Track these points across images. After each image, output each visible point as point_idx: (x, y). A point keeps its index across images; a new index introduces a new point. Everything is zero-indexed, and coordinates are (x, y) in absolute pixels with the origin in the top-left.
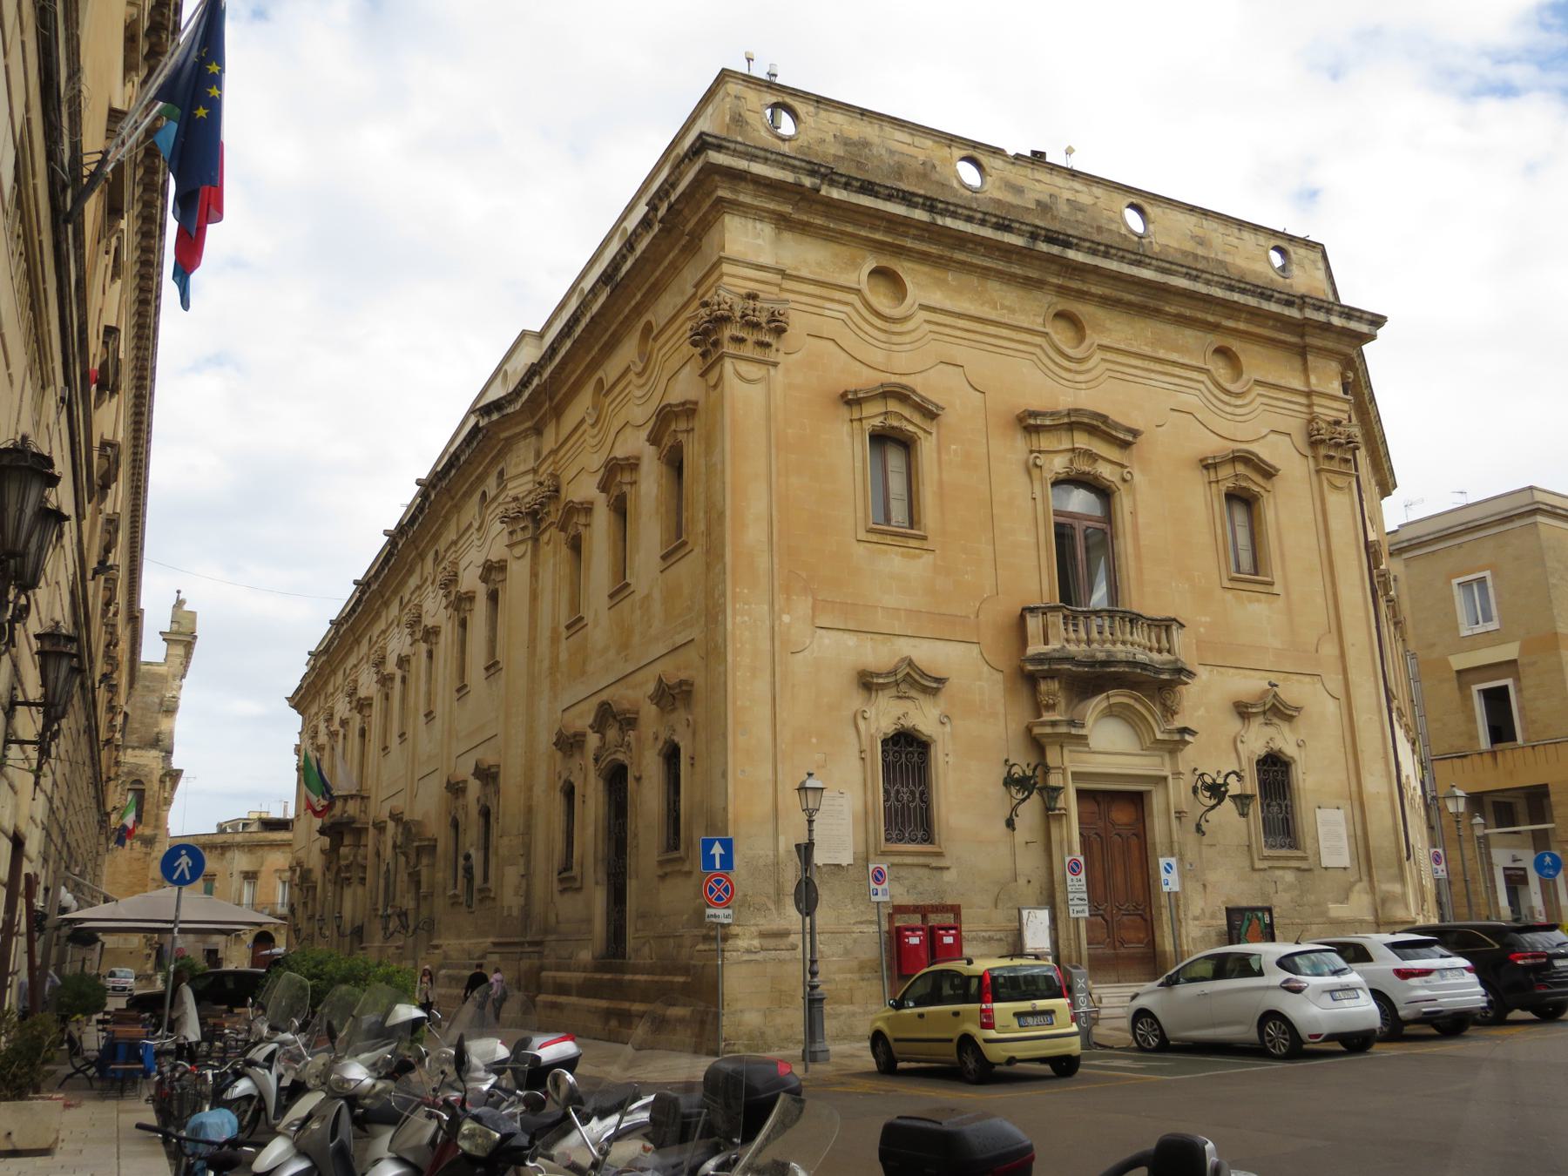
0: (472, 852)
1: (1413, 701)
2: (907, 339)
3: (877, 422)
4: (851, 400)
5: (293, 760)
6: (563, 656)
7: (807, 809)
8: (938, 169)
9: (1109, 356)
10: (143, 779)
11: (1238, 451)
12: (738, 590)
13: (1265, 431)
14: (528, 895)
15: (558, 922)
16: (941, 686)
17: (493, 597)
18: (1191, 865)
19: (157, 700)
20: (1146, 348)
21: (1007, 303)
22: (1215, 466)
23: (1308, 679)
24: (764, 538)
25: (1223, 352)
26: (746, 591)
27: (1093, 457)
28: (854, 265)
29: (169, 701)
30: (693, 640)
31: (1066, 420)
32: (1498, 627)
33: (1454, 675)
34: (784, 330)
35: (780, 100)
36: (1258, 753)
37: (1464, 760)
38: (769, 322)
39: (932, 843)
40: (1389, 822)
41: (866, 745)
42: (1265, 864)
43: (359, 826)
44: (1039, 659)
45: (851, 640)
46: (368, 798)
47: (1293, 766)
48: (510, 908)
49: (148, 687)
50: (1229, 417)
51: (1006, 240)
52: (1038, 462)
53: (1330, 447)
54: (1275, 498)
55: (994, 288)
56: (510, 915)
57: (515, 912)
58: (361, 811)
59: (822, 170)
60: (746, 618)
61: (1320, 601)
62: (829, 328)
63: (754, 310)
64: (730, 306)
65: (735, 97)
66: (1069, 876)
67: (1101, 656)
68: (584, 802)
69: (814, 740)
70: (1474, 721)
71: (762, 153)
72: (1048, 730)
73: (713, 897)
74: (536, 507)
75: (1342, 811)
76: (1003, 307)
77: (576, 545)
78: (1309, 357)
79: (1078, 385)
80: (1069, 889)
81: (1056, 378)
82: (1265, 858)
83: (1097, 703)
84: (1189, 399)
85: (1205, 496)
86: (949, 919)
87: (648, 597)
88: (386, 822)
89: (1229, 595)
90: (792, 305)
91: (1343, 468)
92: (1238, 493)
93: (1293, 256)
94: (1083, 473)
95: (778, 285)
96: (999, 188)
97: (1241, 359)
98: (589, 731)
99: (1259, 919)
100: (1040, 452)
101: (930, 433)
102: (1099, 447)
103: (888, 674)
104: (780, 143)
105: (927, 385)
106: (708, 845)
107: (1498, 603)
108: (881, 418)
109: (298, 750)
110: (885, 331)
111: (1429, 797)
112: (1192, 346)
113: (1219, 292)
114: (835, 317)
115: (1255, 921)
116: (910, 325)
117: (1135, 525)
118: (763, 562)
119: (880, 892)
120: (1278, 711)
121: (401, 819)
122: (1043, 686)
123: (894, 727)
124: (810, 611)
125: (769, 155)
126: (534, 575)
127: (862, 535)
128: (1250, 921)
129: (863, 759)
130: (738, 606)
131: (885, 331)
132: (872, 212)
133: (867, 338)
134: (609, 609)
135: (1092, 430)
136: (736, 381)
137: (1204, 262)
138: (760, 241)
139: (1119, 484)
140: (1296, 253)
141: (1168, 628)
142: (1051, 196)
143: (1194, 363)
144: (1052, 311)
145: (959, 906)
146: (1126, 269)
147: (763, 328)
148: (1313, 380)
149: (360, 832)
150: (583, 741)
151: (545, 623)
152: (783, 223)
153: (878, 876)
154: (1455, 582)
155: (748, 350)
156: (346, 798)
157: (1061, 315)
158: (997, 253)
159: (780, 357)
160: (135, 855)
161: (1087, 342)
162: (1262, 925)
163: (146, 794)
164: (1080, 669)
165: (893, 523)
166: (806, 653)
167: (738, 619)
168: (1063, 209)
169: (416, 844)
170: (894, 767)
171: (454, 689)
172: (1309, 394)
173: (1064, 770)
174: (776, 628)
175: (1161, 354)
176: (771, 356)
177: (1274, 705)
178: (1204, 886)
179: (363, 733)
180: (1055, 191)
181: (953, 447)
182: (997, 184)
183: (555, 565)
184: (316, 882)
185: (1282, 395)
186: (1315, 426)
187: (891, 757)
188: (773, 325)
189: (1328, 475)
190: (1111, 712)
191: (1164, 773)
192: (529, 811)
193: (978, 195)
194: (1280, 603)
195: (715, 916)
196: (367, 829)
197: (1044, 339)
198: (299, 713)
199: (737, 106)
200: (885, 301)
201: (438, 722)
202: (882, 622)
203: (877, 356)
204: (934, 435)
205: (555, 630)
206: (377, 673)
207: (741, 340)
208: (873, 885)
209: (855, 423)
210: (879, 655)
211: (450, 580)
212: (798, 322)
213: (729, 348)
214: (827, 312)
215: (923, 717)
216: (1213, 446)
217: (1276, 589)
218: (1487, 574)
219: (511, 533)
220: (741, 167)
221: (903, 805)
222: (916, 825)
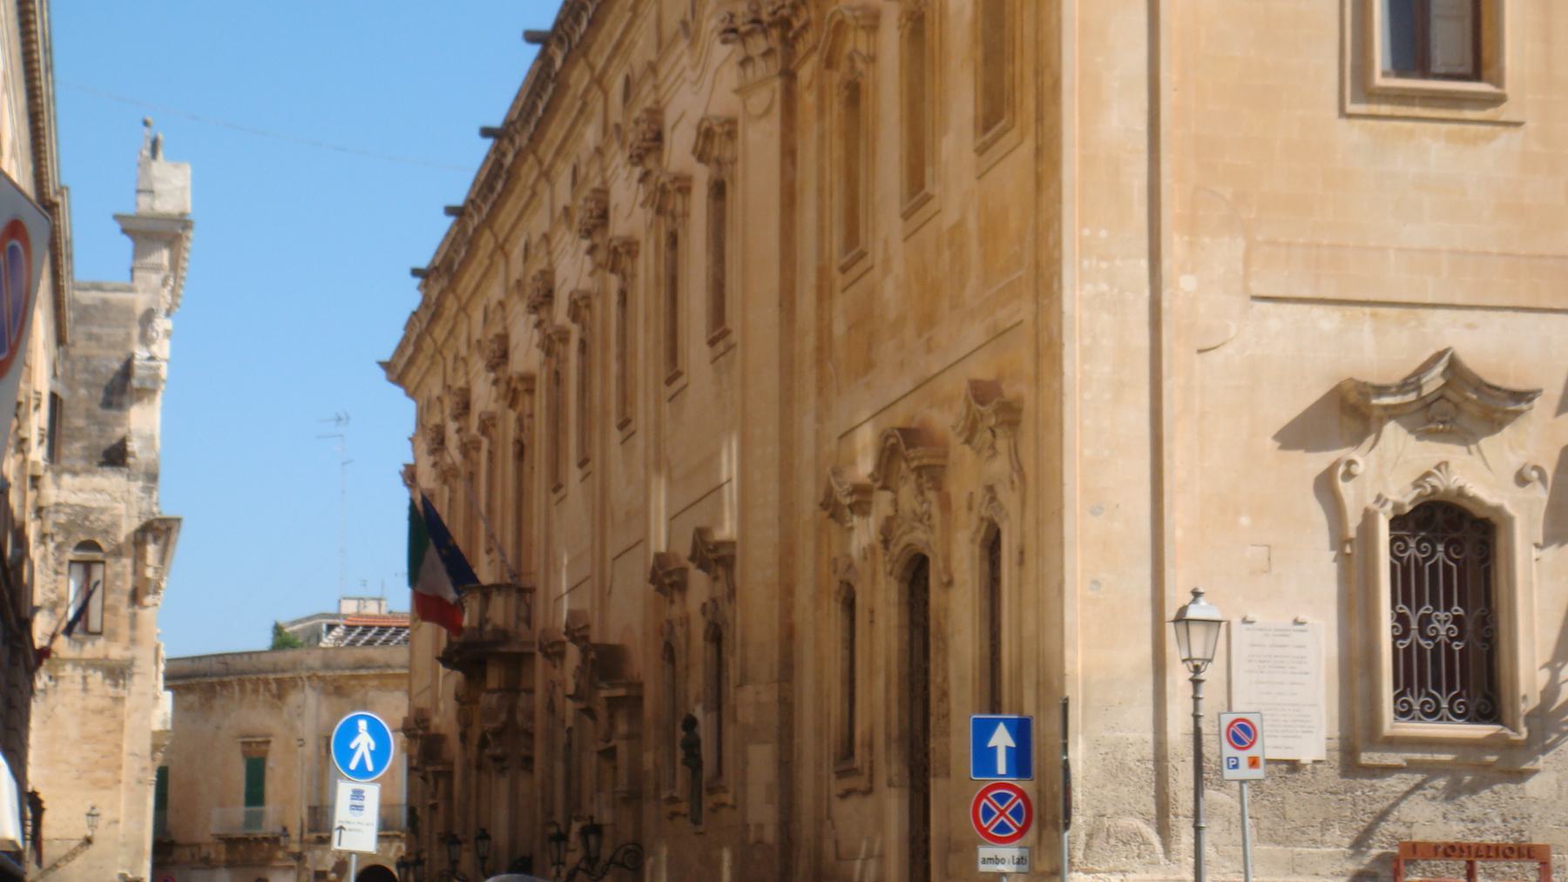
0: (699, 713)
5: (400, 500)
6: (839, 328)
7: (1190, 659)
10: (98, 540)
15: (838, 857)
17: (719, 190)
26: (1103, 233)
30: (1021, 322)
43: (516, 649)
45: (1327, 320)
46: (532, 590)
48: (760, 827)
56: (760, 842)
58: (518, 617)
68: (872, 622)
69: (1245, 521)
73: (990, 825)
77: (854, 93)
87: (959, 226)
88: (562, 643)
98: (692, 567)
106: (984, 730)
109: (410, 476)
121: (586, 638)
124: (1240, 266)
126: (789, 153)
134: (905, 240)
149: (518, 662)
150: (943, 467)
156: (486, 592)
160: (94, 701)
166: (1228, 350)
169: (604, 693)
170: (1419, 571)
171: (663, 378)
179: (521, 451)
183: (822, 137)
184: (451, 764)
187: (1412, 551)
192: (788, 635)
195: (996, 860)
196: (532, 655)
201: (639, 442)
205: (822, 272)
206: (539, 325)
219: (745, 62)
221: (1438, 645)
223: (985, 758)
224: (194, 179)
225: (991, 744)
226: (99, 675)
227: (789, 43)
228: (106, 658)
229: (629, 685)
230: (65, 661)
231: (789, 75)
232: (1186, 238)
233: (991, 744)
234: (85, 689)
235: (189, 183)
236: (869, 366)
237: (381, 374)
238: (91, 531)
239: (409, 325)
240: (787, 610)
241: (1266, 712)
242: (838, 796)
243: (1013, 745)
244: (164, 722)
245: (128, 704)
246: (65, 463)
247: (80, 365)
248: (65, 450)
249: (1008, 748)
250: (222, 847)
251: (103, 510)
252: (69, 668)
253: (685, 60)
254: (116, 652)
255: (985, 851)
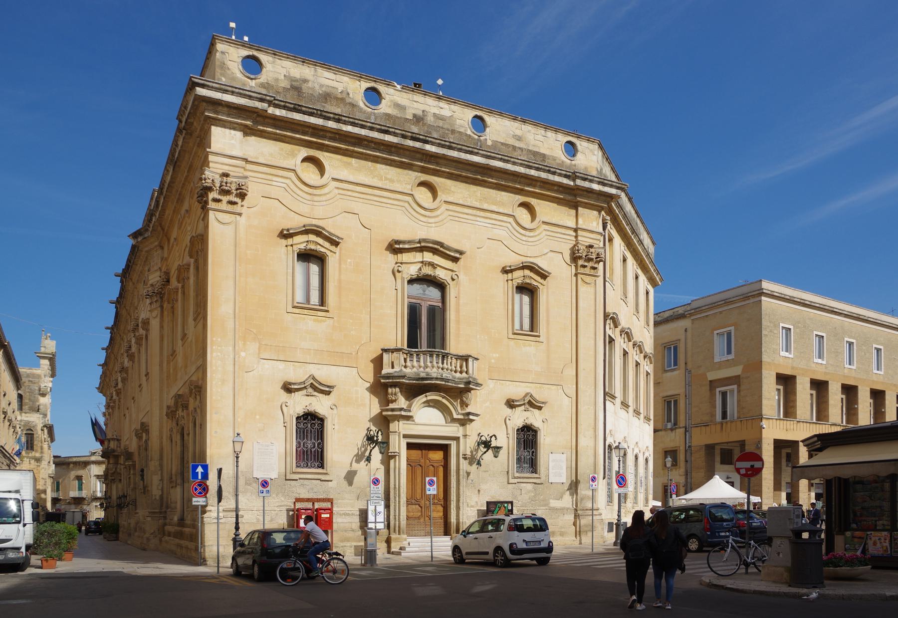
1: (686, 396)
2: (324, 198)
3: (302, 246)
4: (285, 235)
8: (351, 95)
9: (451, 207)
11: (526, 262)
12: (214, 339)
13: (546, 251)
14: (162, 490)
15: (171, 503)
16: (331, 390)
18: (472, 481)
19: (37, 388)
20: (475, 203)
21: (389, 177)
22: (511, 271)
23: (555, 387)
24: (231, 311)
25: (524, 205)
26: (219, 340)
27: (433, 265)
28: (293, 155)
29: (43, 388)
31: (418, 245)
32: (734, 357)
33: (708, 382)
34: (246, 195)
35: (251, 53)
36: (518, 425)
37: (707, 427)
38: (237, 190)
39: (323, 468)
40: (591, 460)
41: (287, 419)
42: (516, 481)
43: (116, 454)
44: (388, 377)
45: (281, 365)
47: (539, 433)
48: (155, 495)
49: (32, 381)
50: (524, 243)
51: (386, 139)
52: (400, 269)
53: (585, 261)
54: (547, 289)
55: (381, 168)
56: (155, 499)
57: (158, 498)
59: (268, 98)
60: (219, 354)
61: (568, 346)
62: (275, 192)
63: (226, 183)
64: (213, 180)
65: (222, 52)
66: (428, 486)
67: (423, 375)
69: (258, 417)
70: (715, 407)
71: (230, 89)
72: (390, 413)
74: (160, 290)
75: (565, 455)
76: (386, 179)
78: (579, 208)
79: (430, 225)
80: (372, 492)
81: (417, 221)
82: (515, 478)
83: (422, 399)
84: (501, 233)
85: (504, 288)
86: (327, 505)
89: (512, 343)
90: (251, 179)
91: (592, 272)
92: (526, 286)
93: (579, 147)
94: (427, 275)
95: (244, 168)
96: (390, 107)
97: (536, 209)
99: (505, 507)
100: (401, 263)
101: (335, 253)
102: (437, 260)
103: (300, 383)
104: (249, 81)
105: (331, 227)
106: (195, 467)
107: (735, 345)
108: (305, 244)
110: (310, 194)
111: (687, 446)
112: (507, 201)
113: (522, 170)
114: (279, 186)
115: (503, 508)
116: (325, 190)
117: (458, 304)
118: (230, 324)
119: (265, 492)
120: (533, 404)
122: (390, 390)
123: (304, 410)
124: (257, 351)
125: (234, 90)
126: (162, 327)
127: (290, 309)
128: (500, 508)
129: (285, 426)
130: (214, 347)
131: (310, 194)
132: (302, 123)
133: (299, 198)
135: (435, 251)
136: (217, 224)
137: (519, 152)
138: (233, 142)
139: (449, 281)
140: (581, 145)
141: (467, 361)
142: (423, 111)
143: (506, 212)
144: (418, 182)
145: (333, 499)
146: (463, 156)
147: (233, 193)
148: (580, 221)
151: (165, 353)
152: (248, 131)
153: (593, 479)
154: (716, 332)
155: (224, 206)
157: (422, 184)
158: (382, 147)
159: (244, 210)
161: (438, 199)
162: (507, 510)
163: (35, 436)
164: (411, 382)
165: (312, 303)
167: (214, 354)
168: (430, 119)
172: (576, 230)
173: (399, 433)
174: (236, 359)
175: (485, 206)
176: (236, 208)
177: (530, 401)
178: (479, 491)
180: (427, 108)
181: (349, 260)
182: (389, 104)
185: (560, 230)
186: (577, 247)
188: (238, 191)
189: (582, 276)
190: (429, 404)
191: (457, 436)
192: (161, 449)
193: (375, 111)
194: (543, 347)
195: (198, 502)
197: (410, 198)
198: (103, 395)
199: (223, 58)
200: (313, 176)
202: (299, 356)
203: (304, 209)
204: (338, 253)
207: (219, 201)
208: (591, 483)
209: (289, 247)
210: (297, 375)
211: (135, 329)
212: (254, 190)
213: (212, 205)
214: (274, 183)
215: (320, 405)
216: (513, 260)
217: (540, 339)
218: (732, 328)
220: (217, 98)
222: (315, 460)
223: (195, 475)
224: (56, 344)
225: (197, 471)
226: (33, 460)
227: (162, 298)
228: (35, 456)
229: (133, 462)
230: (24, 457)
231: (162, 307)
232: (243, 342)
233: (197, 471)
234: (30, 463)
235: (55, 345)
236: (176, 380)
237: (97, 390)
238: (30, 427)
239: (101, 378)
240: (161, 443)
241: (706, 570)
242: (95, 476)
243: (203, 471)
244: (53, 471)
245: (41, 467)
246: (24, 411)
247: (27, 388)
248: (24, 408)
249: (202, 472)
250: (73, 500)
251: (33, 422)
252: (25, 459)
253: (142, 305)
254: (38, 455)
255: (194, 499)
